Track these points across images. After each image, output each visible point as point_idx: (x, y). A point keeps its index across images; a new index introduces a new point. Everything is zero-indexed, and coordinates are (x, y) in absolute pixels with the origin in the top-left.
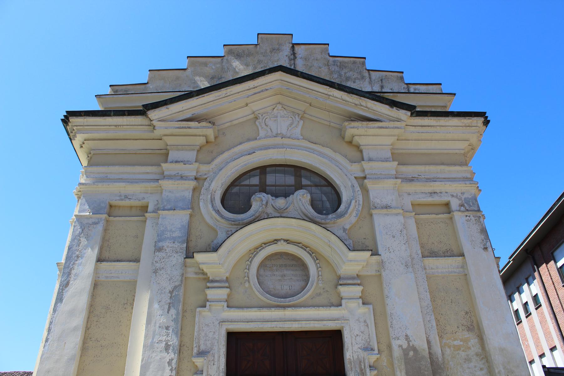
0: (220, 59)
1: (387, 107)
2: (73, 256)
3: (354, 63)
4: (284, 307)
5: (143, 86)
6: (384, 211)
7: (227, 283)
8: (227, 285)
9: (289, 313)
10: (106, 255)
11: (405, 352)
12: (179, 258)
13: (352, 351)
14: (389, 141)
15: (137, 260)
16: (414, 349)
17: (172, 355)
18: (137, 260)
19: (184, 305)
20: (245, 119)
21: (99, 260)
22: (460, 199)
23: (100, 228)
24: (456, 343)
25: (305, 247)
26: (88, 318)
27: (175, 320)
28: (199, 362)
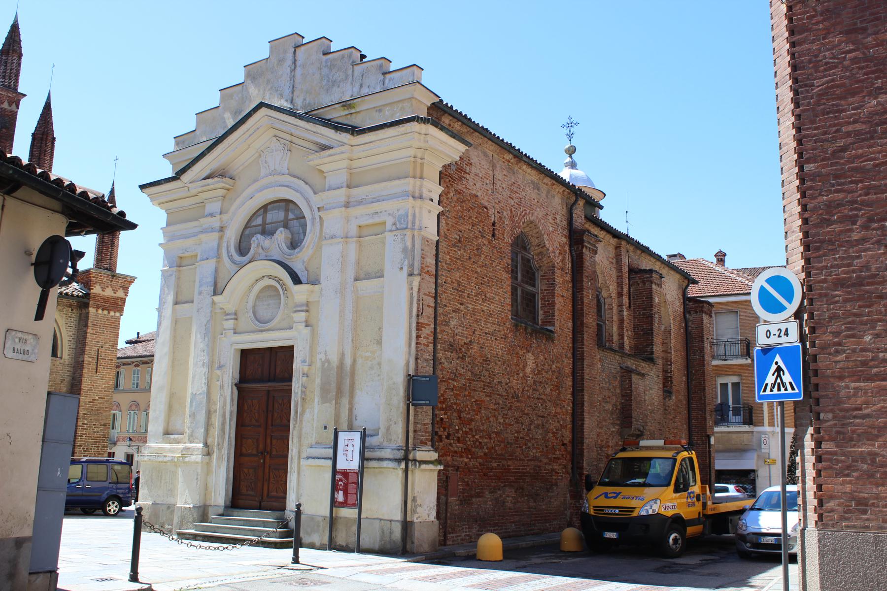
0: (240, 87)
1: (333, 131)
2: (162, 303)
3: (343, 57)
4: (262, 331)
5: (193, 134)
6: (330, 241)
7: (236, 316)
8: (305, 308)
9: (265, 335)
10: (180, 298)
11: (323, 363)
12: (208, 300)
13: (298, 364)
14: (345, 164)
15: (192, 302)
16: (328, 361)
17: (206, 370)
18: (192, 302)
19: (212, 335)
20: (252, 159)
21: (176, 303)
22: (394, 217)
23: (173, 278)
24: (368, 354)
25: (253, 285)
26: (687, 344)
27: (208, 345)
28: (218, 372)
